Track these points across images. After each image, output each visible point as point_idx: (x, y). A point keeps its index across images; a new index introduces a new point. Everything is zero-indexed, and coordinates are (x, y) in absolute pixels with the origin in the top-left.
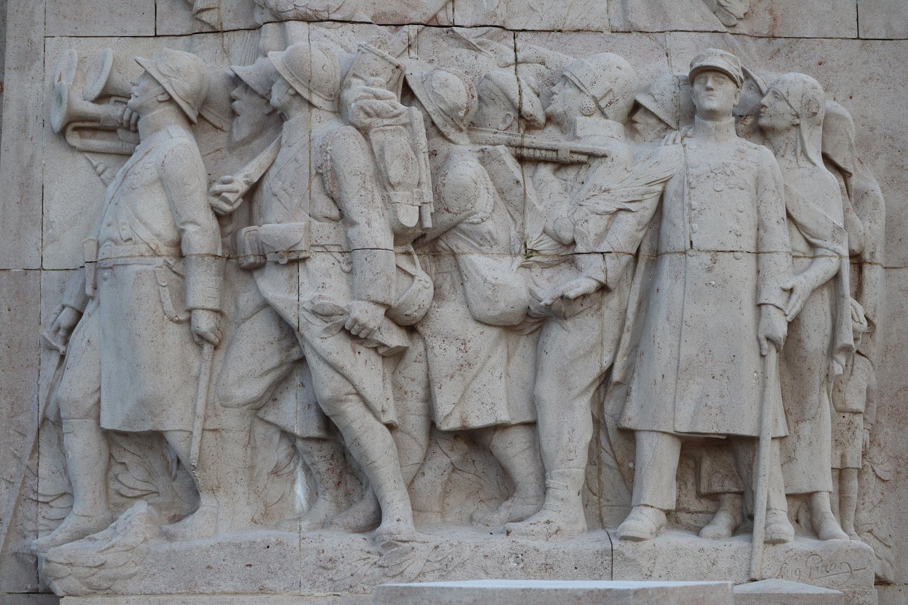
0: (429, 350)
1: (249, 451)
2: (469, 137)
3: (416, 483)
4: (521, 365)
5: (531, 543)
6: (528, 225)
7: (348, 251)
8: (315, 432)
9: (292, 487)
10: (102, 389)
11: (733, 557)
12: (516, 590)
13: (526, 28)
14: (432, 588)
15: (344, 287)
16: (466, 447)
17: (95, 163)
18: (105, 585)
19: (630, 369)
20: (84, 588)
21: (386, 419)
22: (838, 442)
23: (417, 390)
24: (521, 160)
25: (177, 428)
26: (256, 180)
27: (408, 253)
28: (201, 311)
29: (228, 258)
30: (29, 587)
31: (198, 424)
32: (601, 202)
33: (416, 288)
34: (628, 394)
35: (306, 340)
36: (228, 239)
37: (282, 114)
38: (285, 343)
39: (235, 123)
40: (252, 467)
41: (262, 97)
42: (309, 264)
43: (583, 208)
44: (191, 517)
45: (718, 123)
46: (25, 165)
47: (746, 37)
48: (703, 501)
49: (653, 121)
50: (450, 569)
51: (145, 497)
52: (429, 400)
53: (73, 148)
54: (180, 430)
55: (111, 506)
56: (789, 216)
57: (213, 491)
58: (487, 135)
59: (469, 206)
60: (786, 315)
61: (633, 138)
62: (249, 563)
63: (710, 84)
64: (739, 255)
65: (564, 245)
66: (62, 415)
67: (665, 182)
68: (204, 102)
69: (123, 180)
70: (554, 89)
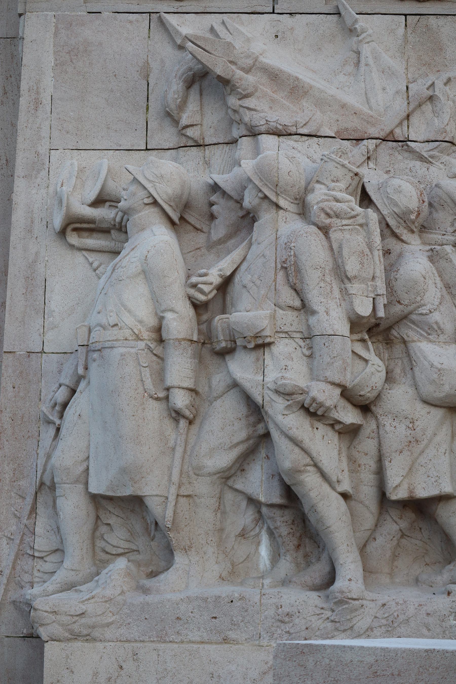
0: (381, 427)
1: (219, 515)
7: (309, 337)
8: (277, 499)
9: (257, 549)
10: (91, 458)
12: (419, 651)
14: (334, 646)
15: (304, 369)
16: (413, 516)
17: (91, 260)
18: (85, 632)
20: (67, 634)
21: (341, 489)
23: (369, 463)
25: (154, 493)
26: (228, 273)
27: (363, 341)
28: (177, 390)
29: (204, 343)
30: (25, 631)
31: (173, 490)
33: (370, 371)
35: (269, 416)
36: (204, 327)
37: (254, 216)
38: (252, 419)
39: (213, 225)
40: (221, 530)
41: (237, 202)
42: (274, 348)
44: (166, 573)
46: (30, 261)
50: (396, 625)
51: (128, 555)
52: (380, 472)
53: (72, 247)
54: (157, 496)
55: (97, 562)
57: (186, 550)
58: (435, 237)
59: (419, 299)
62: (214, 616)
66: (55, 480)
68: (186, 206)
69: (112, 273)
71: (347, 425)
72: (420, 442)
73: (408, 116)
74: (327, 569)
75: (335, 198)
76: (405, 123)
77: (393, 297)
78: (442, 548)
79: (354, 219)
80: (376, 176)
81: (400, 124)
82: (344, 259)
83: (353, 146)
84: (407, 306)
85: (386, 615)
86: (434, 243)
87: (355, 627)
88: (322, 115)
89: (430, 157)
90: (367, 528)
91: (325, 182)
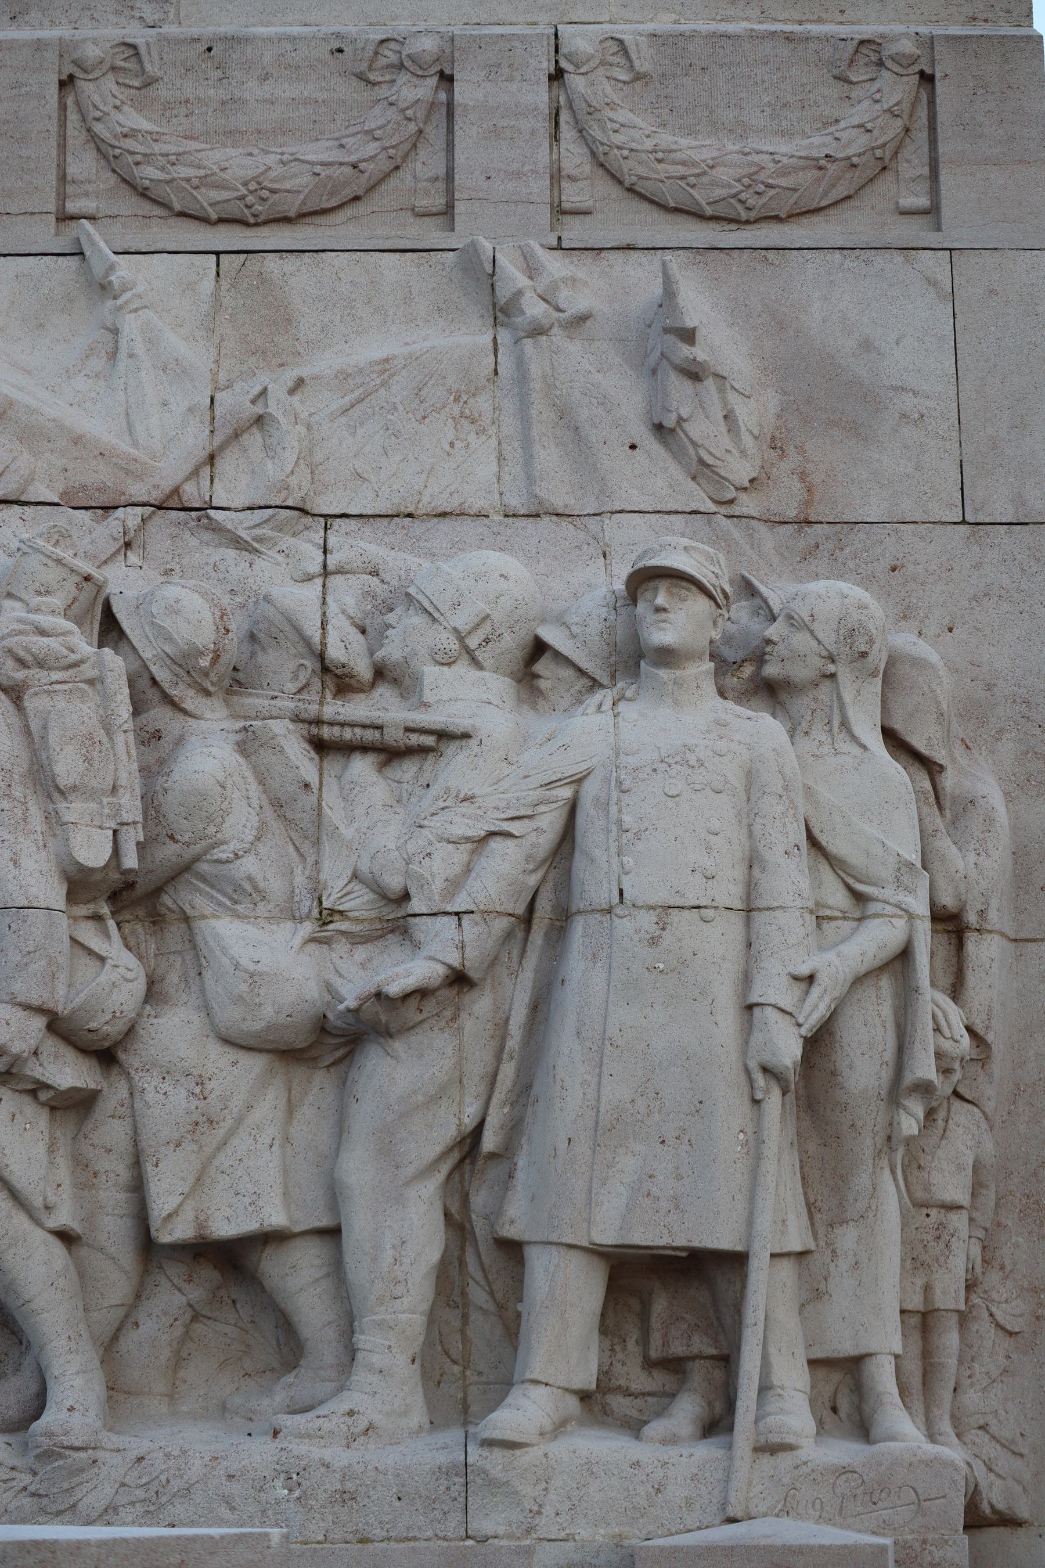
0: (137, 1095)
2: (228, 706)
3: (122, 1341)
4: (311, 1123)
5: (315, 1452)
6: (326, 866)
11: (694, 1477)
13: (349, 511)
16: (215, 1275)
19: (515, 1128)
21: (53, 1223)
22: (916, 1262)
23: (115, 1168)
24: (321, 747)
27: (97, 918)
32: (457, 819)
34: (511, 1176)
43: (424, 831)
45: (678, 673)
47: (754, 522)
48: (655, 1373)
49: (567, 673)
50: (164, 1499)
52: (138, 1187)
56: (813, 842)
59: (212, 829)
60: (799, 1025)
61: (534, 706)
63: (661, 600)
64: (709, 913)
65: (390, 900)
67: (579, 781)
70: (390, 618)
71: (62, 1092)
72: (217, 1123)
73: (212, 458)
74: (34, 1387)
75: (37, 628)
76: (207, 470)
77: (159, 828)
78: (278, 1340)
79: (75, 670)
80: (140, 582)
81: (195, 473)
82: (51, 751)
83: (98, 522)
84: (188, 844)
85: (144, 1481)
86: (253, 714)
87: (80, 1504)
88: (33, 459)
89: (254, 539)
90: (113, 1302)
91: (23, 596)
